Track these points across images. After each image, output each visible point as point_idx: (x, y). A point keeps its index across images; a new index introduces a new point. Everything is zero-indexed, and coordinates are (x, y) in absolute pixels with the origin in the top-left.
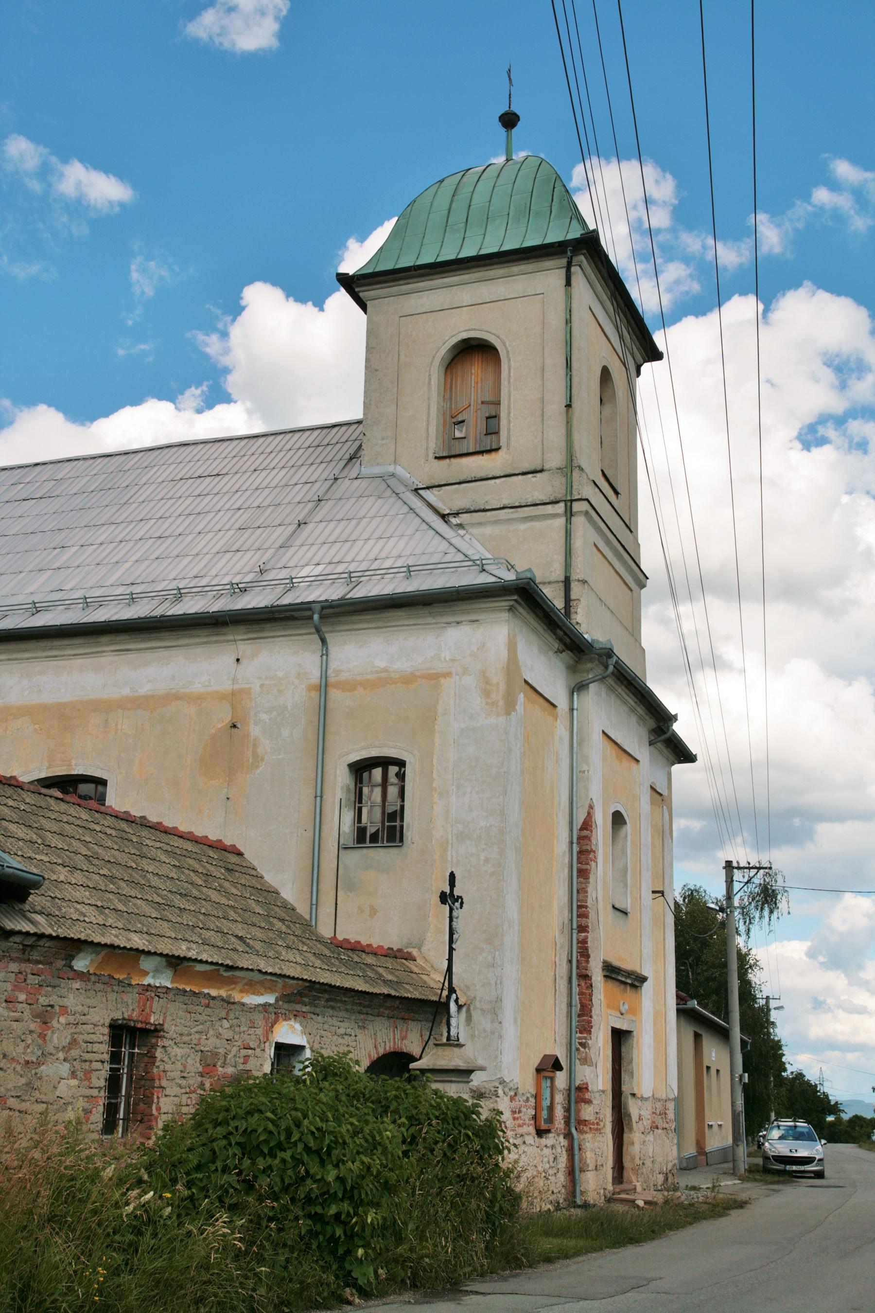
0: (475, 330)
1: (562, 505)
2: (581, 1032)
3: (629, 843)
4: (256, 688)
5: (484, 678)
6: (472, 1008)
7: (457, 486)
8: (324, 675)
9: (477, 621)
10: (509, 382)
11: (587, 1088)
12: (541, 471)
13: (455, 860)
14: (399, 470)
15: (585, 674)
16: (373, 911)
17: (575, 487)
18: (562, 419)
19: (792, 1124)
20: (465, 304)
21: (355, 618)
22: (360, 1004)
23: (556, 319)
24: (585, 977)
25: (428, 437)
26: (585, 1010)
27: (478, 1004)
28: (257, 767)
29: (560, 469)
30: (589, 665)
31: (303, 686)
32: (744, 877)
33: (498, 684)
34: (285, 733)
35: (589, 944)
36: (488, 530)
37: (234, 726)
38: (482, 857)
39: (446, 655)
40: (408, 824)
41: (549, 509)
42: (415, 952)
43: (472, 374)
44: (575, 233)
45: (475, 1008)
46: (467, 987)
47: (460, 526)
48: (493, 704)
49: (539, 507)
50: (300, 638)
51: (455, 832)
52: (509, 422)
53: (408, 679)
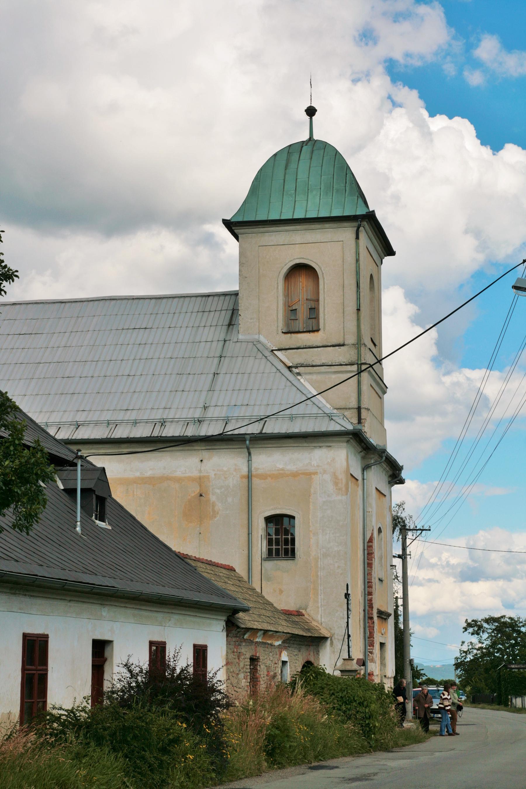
0: (303, 258)
1: (356, 366)
2: (369, 646)
3: (383, 543)
4: (212, 475)
5: (335, 476)
6: (333, 638)
7: (296, 350)
8: (249, 470)
9: (330, 446)
10: (324, 292)
11: (373, 674)
12: (343, 345)
13: (322, 567)
14: (262, 339)
15: (369, 460)
16: (281, 591)
17: (362, 356)
18: (355, 316)
19: (435, 688)
20: (297, 243)
21: (265, 442)
22: (300, 641)
23: (350, 258)
24: (371, 618)
25: (277, 320)
26: (371, 635)
27: (336, 636)
28: (215, 517)
29: (353, 345)
30: (372, 456)
31: (238, 476)
32: (413, 535)
33: (342, 479)
34: (230, 500)
35: (373, 602)
36: (314, 377)
37: (201, 495)
38: (336, 566)
39: (314, 463)
40: (298, 548)
41: (349, 368)
42: (303, 612)
43: (300, 282)
44: (361, 211)
45: (335, 639)
46: (330, 628)
47: (299, 374)
48: (339, 489)
49: (343, 366)
50: (235, 450)
51: (322, 553)
52: (324, 315)
53: (295, 475)
